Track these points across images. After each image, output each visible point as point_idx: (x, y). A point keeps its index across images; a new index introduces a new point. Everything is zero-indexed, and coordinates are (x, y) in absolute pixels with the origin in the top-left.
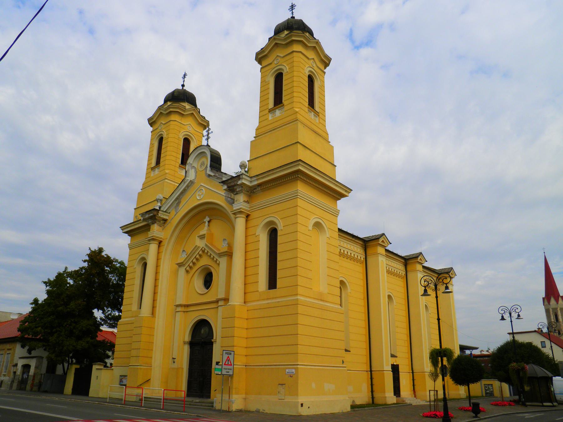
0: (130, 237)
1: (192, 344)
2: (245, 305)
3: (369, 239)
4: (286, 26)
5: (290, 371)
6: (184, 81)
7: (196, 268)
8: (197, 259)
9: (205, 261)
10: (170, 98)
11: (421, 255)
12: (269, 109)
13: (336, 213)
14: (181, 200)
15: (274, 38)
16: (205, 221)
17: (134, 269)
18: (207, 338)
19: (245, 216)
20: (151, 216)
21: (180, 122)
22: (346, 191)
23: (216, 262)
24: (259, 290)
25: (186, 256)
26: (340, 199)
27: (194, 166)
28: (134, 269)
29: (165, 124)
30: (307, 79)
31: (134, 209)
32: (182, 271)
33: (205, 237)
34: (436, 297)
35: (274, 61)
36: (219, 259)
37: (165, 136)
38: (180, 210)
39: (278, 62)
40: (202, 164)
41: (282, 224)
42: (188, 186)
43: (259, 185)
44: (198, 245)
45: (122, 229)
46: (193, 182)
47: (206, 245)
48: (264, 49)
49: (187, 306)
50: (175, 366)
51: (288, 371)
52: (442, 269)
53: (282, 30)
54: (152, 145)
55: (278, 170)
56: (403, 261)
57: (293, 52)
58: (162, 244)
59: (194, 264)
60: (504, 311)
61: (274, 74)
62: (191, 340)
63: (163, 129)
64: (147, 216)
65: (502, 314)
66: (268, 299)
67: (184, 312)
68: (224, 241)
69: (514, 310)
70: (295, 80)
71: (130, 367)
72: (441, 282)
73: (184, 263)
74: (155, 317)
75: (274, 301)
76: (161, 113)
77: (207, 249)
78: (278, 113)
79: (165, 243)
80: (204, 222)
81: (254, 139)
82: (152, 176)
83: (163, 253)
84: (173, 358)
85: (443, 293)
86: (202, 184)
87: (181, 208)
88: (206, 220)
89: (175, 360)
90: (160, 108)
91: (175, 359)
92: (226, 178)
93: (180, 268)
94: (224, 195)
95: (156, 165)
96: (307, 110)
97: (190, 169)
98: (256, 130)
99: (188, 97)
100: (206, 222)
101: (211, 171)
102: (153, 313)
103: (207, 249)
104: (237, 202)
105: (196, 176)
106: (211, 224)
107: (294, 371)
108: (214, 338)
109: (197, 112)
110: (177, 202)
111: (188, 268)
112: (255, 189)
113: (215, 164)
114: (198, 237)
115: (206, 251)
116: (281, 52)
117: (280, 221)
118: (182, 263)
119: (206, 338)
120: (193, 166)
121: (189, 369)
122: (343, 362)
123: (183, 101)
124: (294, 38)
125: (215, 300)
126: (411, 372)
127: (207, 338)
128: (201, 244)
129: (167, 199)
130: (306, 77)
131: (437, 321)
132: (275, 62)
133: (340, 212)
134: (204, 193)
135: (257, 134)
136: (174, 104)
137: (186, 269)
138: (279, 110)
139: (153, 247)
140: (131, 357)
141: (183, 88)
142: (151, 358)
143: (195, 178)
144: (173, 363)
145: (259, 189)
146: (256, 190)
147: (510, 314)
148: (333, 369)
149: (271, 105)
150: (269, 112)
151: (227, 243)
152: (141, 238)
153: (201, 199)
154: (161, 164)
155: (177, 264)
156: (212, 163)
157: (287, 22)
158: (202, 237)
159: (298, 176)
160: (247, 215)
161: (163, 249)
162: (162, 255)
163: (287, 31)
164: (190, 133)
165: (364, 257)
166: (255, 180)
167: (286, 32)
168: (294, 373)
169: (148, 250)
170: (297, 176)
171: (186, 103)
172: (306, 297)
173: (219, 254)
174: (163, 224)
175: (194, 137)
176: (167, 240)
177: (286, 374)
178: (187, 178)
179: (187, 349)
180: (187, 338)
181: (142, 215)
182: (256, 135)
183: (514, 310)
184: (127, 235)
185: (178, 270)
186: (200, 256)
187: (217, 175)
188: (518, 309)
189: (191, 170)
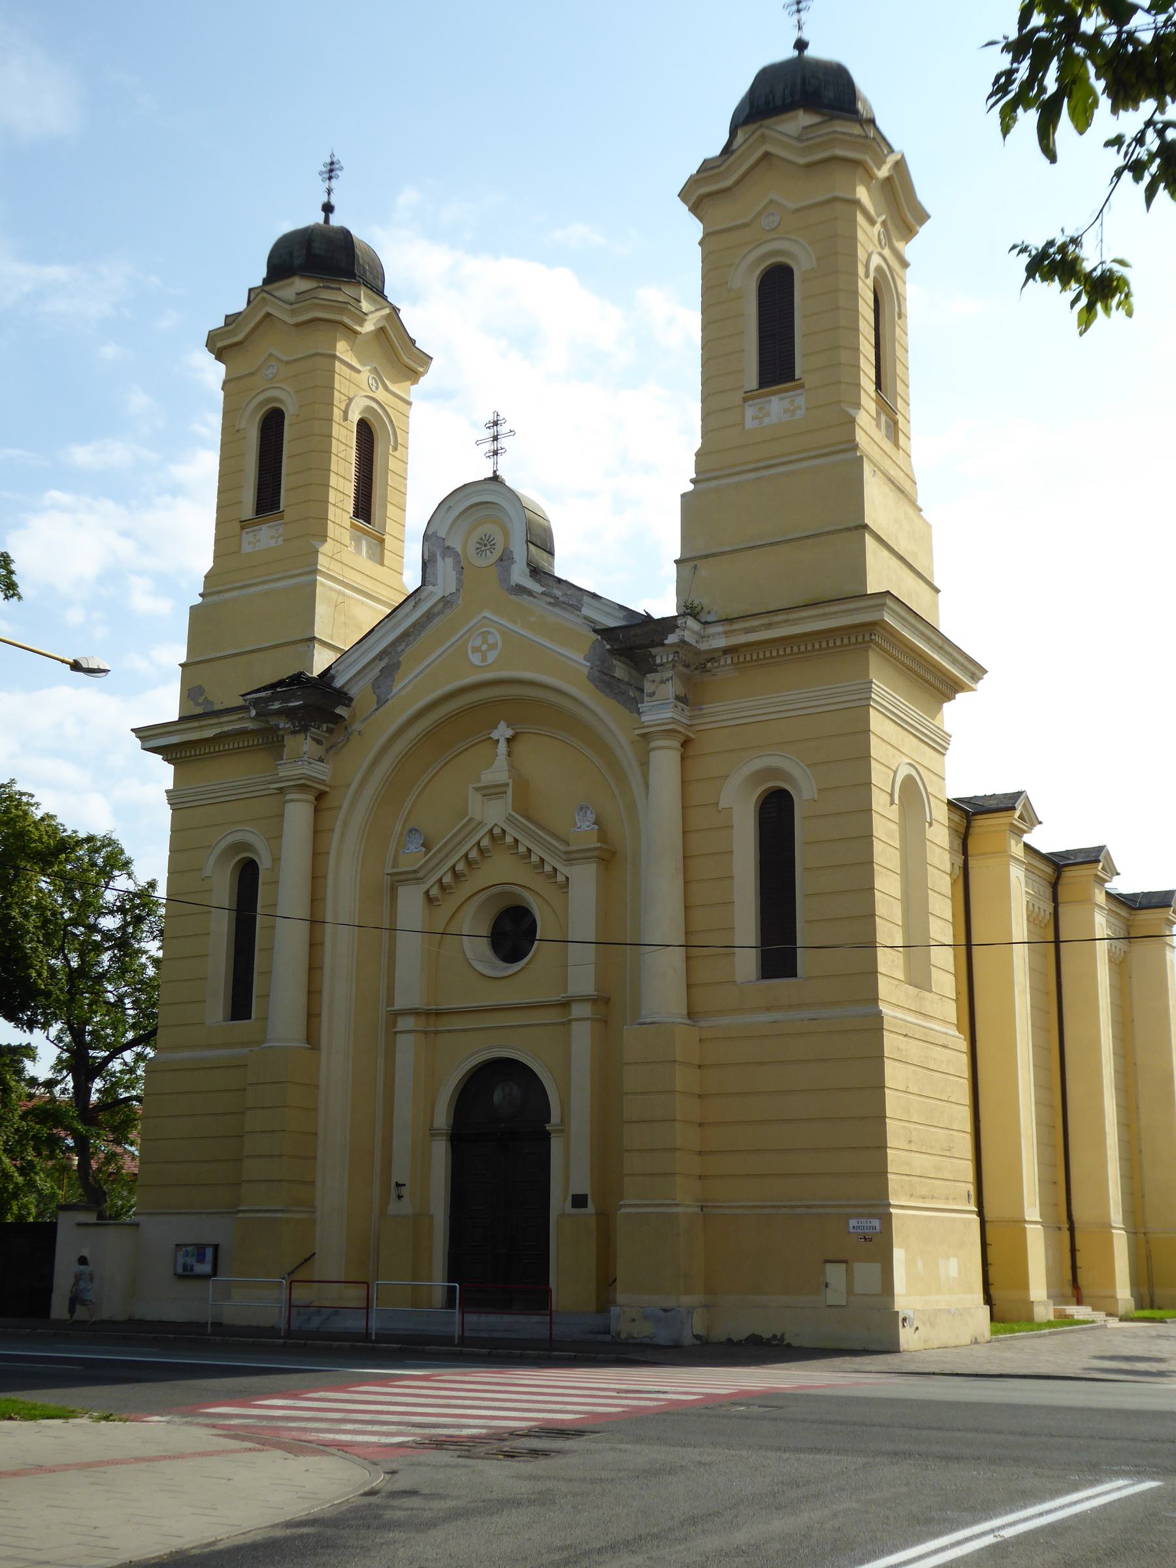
0: (172, 767)
5: (865, 1225)
6: (329, 192)
8: (469, 863)
12: (745, 392)
13: (939, 744)
16: (495, 735)
29: (288, 363)
36: (563, 869)
46: (449, 602)
51: (856, 1225)
53: (779, 103)
55: (805, 613)
59: (456, 875)
73: (421, 874)
76: (268, 315)
83: (336, 835)
89: (405, 1191)
91: (404, 1185)
97: (439, 558)
100: (498, 741)
102: (312, 1037)
104: (655, 698)
105: (460, 581)
108: (555, 1117)
110: (383, 664)
111: (434, 892)
112: (712, 660)
117: (808, 771)
120: (448, 548)
124: (840, 152)
133: (951, 739)
137: (427, 893)
139: (298, 814)
141: (327, 220)
142: (313, 1183)
143: (458, 590)
145: (729, 661)
146: (716, 664)
148: (662, 1213)
149: (751, 376)
150: (745, 400)
151: (593, 820)
153: (485, 666)
160: (682, 740)
168: (878, 1230)
173: (566, 853)
174: (327, 735)
179: (440, 1153)
180: (442, 1118)
189: (443, 558)
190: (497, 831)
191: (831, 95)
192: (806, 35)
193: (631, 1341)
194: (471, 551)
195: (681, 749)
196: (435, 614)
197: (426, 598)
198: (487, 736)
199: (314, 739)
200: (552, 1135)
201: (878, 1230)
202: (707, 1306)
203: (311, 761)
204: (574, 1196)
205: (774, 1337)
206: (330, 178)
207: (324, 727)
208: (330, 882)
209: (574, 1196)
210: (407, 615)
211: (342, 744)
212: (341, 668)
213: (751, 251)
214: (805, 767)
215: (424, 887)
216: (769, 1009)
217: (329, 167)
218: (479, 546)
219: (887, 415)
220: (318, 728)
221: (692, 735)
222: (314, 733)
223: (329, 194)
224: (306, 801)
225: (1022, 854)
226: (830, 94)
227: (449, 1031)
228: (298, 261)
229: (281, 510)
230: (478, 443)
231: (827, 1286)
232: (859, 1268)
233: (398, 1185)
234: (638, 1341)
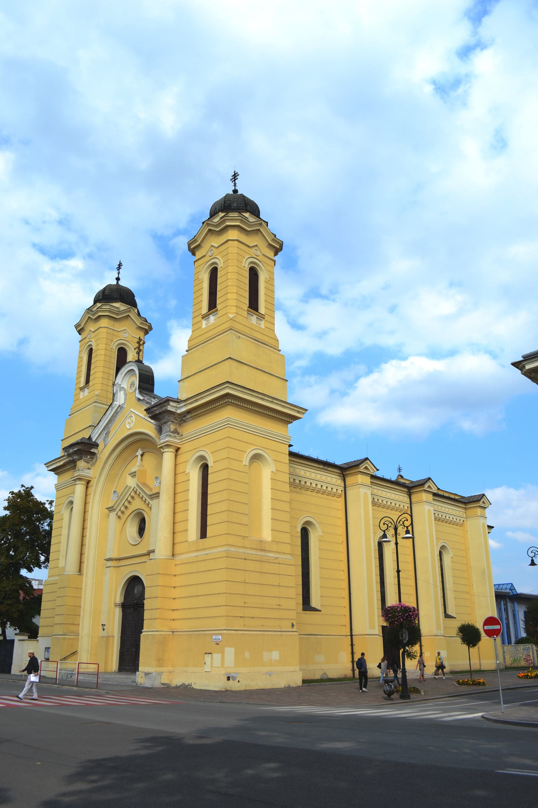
0: (57, 476)
1: (124, 606)
2: (173, 558)
3: (349, 466)
4: (223, 206)
6: (119, 273)
7: (128, 513)
9: (137, 504)
10: (100, 298)
11: (430, 481)
12: (202, 316)
14: (111, 429)
15: (207, 223)
16: (137, 454)
17: (61, 515)
18: (140, 599)
19: (174, 451)
20: (75, 451)
21: (113, 328)
22: (299, 412)
23: (148, 505)
24: (59, 566)
25: (117, 498)
26: (291, 423)
27: (123, 386)
28: (61, 515)
30: (247, 274)
31: (61, 440)
32: (113, 515)
33: (136, 475)
34: (395, 544)
35: (207, 252)
36: (150, 502)
37: (95, 346)
38: (109, 442)
39: (212, 254)
40: (132, 385)
41: (211, 460)
42: (116, 413)
43: (189, 412)
44: (129, 485)
45: (47, 465)
46: (122, 407)
47: (138, 485)
48: (196, 238)
49: (120, 559)
50: (105, 633)
51: (215, 638)
52: (472, 496)
54: (81, 358)
56: (406, 490)
57: (228, 241)
58: (90, 484)
60: (535, 553)
61: (88, 349)
62: (124, 602)
63: (92, 338)
64: (71, 451)
65: (532, 558)
66: (197, 551)
67: (115, 567)
68: (156, 480)
69: (401, 523)
71: (53, 637)
72: (401, 525)
73: (115, 508)
74: (83, 575)
75: (203, 553)
76: (89, 317)
77: (139, 491)
78: (212, 318)
79: (93, 483)
80: (137, 456)
81: (186, 353)
82: (81, 398)
83: (92, 495)
84: (102, 625)
85: (403, 538)
86: (131, 410)
87: (110, 440)
88: (139, 454)
89: (105, 627)
90: (87, 312)
91: (105, 625)
92: (147, 406)
93: (111, 514)
94: (154, 424)
95: (86, 384)
96: (245, 314)
97: (119, 391)
98: (188, 341)
99: (122, 294)
101: (140, 394)
103: (139, 491)
105: (125, 399)
106: (144, 457)
107: (220, 637)
109: (135, 314)
112: (185, 416)
113: (145, 385)
114: (129, 474)
115: (138, 492)
116: (215, 241)
118: (112, 507)
119: (139, 599)
120: (122, 387)
121: (121, 637)
122: (293, 625)
123: (115, 300)
124: (228, 223)
125: (146, 552)
127: (140, 599)
128: (131, 482)
130: (245, 272)
131: (397, 573)
132: (209, 254)
134: (134, 420)
135: (190, 347)
136: (104, 307)
137: (117, 514)
138: (213, 316)
139: (80, 488)
140: (55, 625)
141: (118, 282)
142: (78, 625)
143: (125, 402)
144: (103, 630)
147: (396, 529)
149: (205, 309)
150: (203, 318)
152: (67, 476)
154: (90, 383)
155: (107, 508)
156: (141, 384)
157: (224, 200)
158: (133, 474)
159: (228, 400)
161: (91, 490)
162: (90, 499)
163: (222, 212)
164: (258, 259)
165: (343, 489)
166: (183, 406)
167: (221, 214)
169: (74, 492)
170: (226, 401)
171: (120, 303)
172: (239, 547)
173: (150, 495)
175: (132, 345)
176: (96, 479)
177: (213, 641)
178: (115, 403)
179: (118, 613)
180: (119, 599)
181: (65, 449)
182: (188, 348)
183: (401, 523)
184: (54, 473)
185: (108, 516)
187: (146, 399)
188: (407, 520)
191: (235, 205)
195: (176, 452)
196: (118, 412)
197: (114, 407)
198: (135, 455)
199: (84, 461)
203: (83, 469)
205: (189, 684)
207: (89, 457)
208: (90, 513)
210: (110, 413)
212: (93, 435)
213: (206, 264)
214: (209, 454)
215: (116, 512)
218: (131, 385)
220: (86, 457)
221: (180, 446)
222: (84, 459)
223: (119, 275)
224: (84, 484)
227: (122, 566)
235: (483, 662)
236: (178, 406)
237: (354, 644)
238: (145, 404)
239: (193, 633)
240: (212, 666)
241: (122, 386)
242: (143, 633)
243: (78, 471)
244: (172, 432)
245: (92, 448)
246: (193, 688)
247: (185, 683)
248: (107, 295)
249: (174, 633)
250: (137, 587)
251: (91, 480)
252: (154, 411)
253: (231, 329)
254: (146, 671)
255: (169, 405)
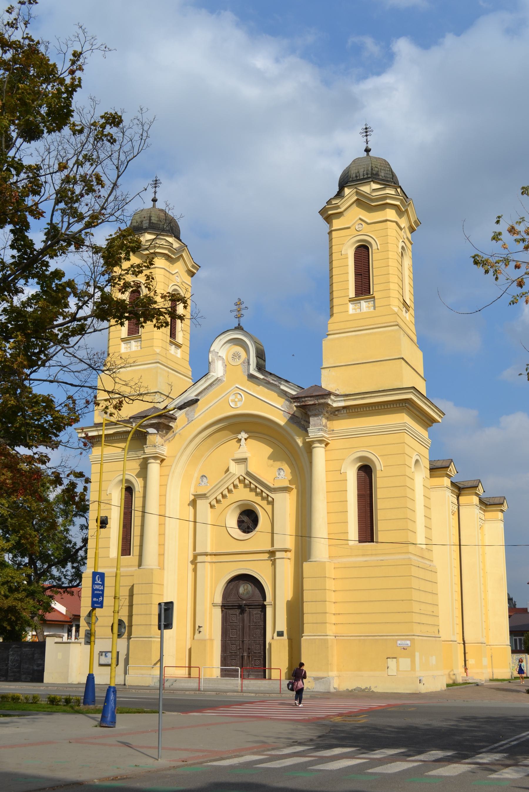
1: (225, 607)
6: (155, 192)
27: (221, 355)
51: (400, 643)
59: (224, 496)
70: (390, 264)
75: (374, 558)
77: (248, 480)
97: (216, 361)
100: (241, 439)
105: (225, 371)
111: (214, 502)
118: (205, 494)
126: (463, 642)
129: (174, 399)
141: (154, 206)
143: (224, 375)
166: (342, 400)
168: (409, 645)
179: (218, 613)
180: (219, 600)
186: (235, 486)
190: (241, 478)
191: (383, 174)
192: (370, 146)
193: (308, 690)
194: (230, 359)
200: (267, 606)
201: (409, 645)
202: (339, 677)
204: (278, 632)
206: (156, 187)
209: (278, 632)
211: (172, 438)
215: (209, 501)
216: (363, 555)
217: (155, 182)
218: (233, 356)
219: (406, 308)
220: (162, 432)
223: (155, 194)
225: (450, 486)
226: (382, 174)
228: (145, 224)
229: (140, 334)
230: (231, 311)
231: (388, 668)
232: (401, 660)
233: (199, 627)
234: (311, 690)
235: (495, 671)
236: (335, 399)
237: (466, 652)
238: (264, 384)
239: (366, 638)
240: (398, 669)
241: (219, 355)
242: (304, 638)
243: (153, 447)
244: (324, 426)
245: (171, 422)
246: (373, 692)
247: (360, 687)
248: (155, 223)
249: (337, 637)
250: (244, 587)
251: (165, 459)
252: (306, 400)
253: (397, 325)
254: (315, 676)
255: (330, 398)
